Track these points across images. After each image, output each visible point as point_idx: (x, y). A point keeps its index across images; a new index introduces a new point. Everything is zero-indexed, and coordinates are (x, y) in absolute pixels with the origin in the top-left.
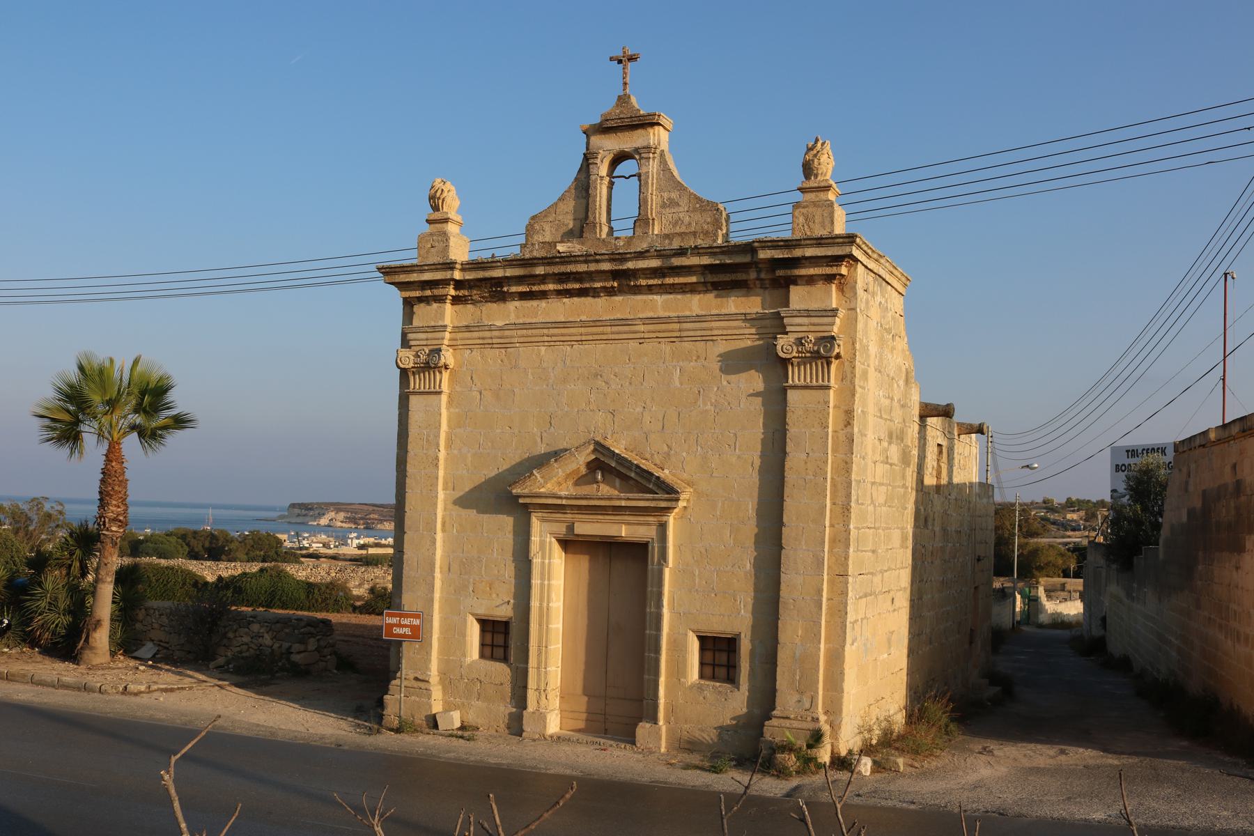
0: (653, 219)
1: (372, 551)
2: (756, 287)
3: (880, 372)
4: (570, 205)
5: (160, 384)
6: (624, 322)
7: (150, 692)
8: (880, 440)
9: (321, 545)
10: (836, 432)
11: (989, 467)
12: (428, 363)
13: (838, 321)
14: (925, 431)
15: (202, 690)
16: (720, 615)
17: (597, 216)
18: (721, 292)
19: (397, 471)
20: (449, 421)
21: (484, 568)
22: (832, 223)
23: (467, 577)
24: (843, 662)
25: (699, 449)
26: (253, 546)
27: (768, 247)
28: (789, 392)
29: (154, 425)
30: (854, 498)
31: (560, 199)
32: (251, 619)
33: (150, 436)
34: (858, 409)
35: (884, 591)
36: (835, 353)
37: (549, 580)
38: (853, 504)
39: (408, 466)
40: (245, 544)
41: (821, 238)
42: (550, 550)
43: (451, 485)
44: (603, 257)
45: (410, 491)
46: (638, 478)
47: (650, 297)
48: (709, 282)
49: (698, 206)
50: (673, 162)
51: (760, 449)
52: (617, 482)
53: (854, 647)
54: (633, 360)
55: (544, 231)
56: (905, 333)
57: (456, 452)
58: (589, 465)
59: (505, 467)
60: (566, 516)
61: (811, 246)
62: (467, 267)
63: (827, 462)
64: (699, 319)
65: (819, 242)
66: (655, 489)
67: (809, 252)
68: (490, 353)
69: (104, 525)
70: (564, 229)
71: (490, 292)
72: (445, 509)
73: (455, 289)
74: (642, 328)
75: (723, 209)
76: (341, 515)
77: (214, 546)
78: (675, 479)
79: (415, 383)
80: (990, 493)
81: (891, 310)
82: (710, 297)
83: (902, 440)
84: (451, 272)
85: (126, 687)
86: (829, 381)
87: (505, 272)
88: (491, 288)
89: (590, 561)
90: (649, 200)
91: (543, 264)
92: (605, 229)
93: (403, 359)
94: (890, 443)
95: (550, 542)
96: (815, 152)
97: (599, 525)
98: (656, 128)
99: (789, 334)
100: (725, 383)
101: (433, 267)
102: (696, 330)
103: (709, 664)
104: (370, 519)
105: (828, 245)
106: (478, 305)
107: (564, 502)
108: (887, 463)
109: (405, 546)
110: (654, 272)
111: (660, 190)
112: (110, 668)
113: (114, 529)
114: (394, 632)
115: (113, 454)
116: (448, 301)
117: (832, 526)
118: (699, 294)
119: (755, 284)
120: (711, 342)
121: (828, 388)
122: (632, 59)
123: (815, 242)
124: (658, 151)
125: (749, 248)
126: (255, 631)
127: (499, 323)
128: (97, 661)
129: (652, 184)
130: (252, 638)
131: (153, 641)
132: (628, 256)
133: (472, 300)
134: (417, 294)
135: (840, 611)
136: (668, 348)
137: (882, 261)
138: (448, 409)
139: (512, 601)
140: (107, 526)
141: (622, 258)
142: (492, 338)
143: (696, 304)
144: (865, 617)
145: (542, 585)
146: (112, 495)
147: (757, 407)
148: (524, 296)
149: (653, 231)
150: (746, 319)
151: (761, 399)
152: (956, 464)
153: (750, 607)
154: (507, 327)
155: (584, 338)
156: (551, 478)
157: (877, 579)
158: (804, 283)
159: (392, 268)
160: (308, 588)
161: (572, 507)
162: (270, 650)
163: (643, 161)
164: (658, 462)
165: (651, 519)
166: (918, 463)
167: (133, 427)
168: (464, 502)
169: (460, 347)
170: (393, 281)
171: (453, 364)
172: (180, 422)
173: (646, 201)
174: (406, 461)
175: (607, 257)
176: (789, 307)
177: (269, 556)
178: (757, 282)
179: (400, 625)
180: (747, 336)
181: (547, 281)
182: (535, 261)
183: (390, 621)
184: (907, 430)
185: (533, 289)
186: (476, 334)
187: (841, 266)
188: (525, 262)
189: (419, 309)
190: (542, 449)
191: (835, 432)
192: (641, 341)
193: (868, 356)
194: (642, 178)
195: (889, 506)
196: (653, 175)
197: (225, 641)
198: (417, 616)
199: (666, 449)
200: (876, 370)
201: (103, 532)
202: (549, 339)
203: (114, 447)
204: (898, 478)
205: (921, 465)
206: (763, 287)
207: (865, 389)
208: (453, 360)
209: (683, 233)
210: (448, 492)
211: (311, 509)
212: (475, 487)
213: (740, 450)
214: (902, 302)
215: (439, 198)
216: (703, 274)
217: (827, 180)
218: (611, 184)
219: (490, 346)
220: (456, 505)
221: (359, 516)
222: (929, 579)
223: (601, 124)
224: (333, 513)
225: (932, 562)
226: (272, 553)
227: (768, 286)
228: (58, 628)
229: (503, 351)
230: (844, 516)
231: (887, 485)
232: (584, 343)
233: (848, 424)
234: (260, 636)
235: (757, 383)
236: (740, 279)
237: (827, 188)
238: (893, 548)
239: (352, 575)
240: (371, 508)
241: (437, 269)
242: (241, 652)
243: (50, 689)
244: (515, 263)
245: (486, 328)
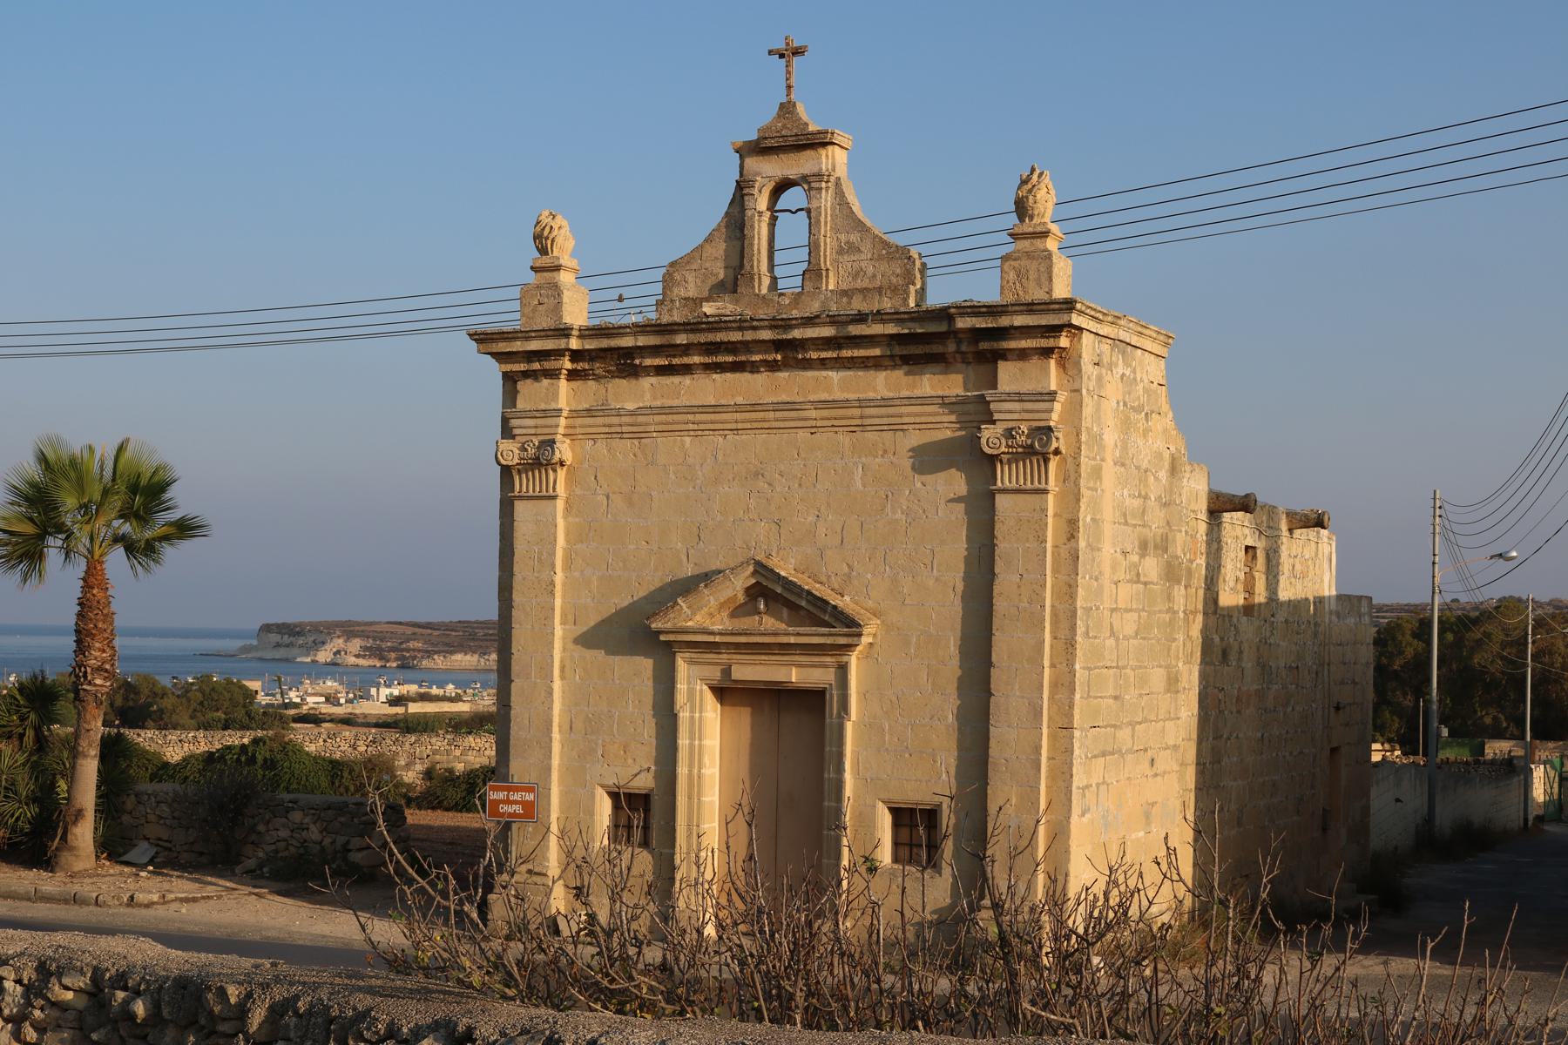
0: (827, 270)
1: (414, 708)
3: (1123, 465)
4: (719, 248)
5: (156, 479)
6: (790, 406)
7: (165, 903)
8: (1124, 553)
9: (323, 699)
10: (1057, 547)
11: (1437, 558)
12: (538, 458)
13: (1057, 406)
14: (1219, 530)
15: (234, 899)
16: (916, 781)
17: (755, 264)
18: (912, 368)
20: (567, 534)
21: (615, 726)
22: (1050, 280)
23: (594, 737)
24: (1069, 837)
25: (887, 568)
26: (201, 703)
27: (967, 313)
28: (998, 497)
29: (148, 534)
30: (1080, 630)
31: (706, 240)
32: (290, 805)
33: (142, 551)
34: (1086, 517)
35: (1136, 748)
36: (1052, 448)
37: (700, 739)
38: (1079, 638)
39: (514, 593)
40: (189, 700)
41: (1033, 304)
42: (701, 700)
43: (571, 617)
44: (762, 323)
45: (518, 626)
47: (824, 373)
49: (884, 252)
50: (853, 191)
51: (963, 569)
52: (785, 612)
53: (1084, 820)
54: (803, 455)
55: (686, 282)
56: (1168, 406)
57: (577, 574)
58: (748, 590)
59: (642, 594)
60: (721, 656)
61: (1021, 312)
62: (588, 333)
63: (1045, 585)
64: (885, 402)
65: (1031, 308)
66: (831, 621)
67: (1019, 321)
68: (616, 443)
69: (85, 676)
70: (712, 281)
71: (618, 365)
72: (564, 650)
73: (572, 361)
74: (813, 414)
75: (916, 256)
76: (356, 645)
77: (131, 703)
78: (857, 608)
79: (521, 484)
81: (1142, 381)
82: (898, 375)
83: (1166, 550)
84: (565, 340)
85: (132, 897)
86: (1046, 483)
87: (636, 340)
88: (619, 360)
89: (752, 714)
90: (822, 244)
91: (686, 331)
92: (766, 281)
93: (504, 454)
94: (1143, 556)
95: (701, 691)
96: (1030, 186)
97: (762, 666)
98: (830, 148)
99: (998, 423)
100: (919, 485)
101: (542, 334)
102: (882, 417)
103: (905, 844)
104: (408, 650)
106: (603, 381)
107: (718, 639)
108: (1138, 582)
109: (513, 699)
110: (828, 343)
111: (836, 230)
112: (98, 875)
113: (98, 682)
115: (92, 579)
116: (562, 376)
117: (1053, 666)
118: (886, 370)
119: (954, 358)
120: (901, 433)
121: (1045, 492)
122: (798, 52)
123: (1025, 308)
124: (832, 179)
125: (944, 314)
126: (297, 821)
127: (630, 406)
128: (79, 866)
129: (826, 223)
130: (292, 831)
131: (148, 839)
132: (794, 322)
133: (594, 374)
134: (522, 367)
135: (1063, 774)
136: (847, 440)
137: (1122, 322)
138: (565, 518)
139: (653, 768)
140: (89, 678)
141: (787, 325)
142: (621, 425)
143: (883, 383)
144: (1103, 783)
145: (691, 746)
146: (94, 635)
147: (959, 516)
148: (661, 371)
149: (827, 285)
150: (944, 404)
151: (963, 505)
152: (1286, 571)
153: (953, 771)
154: (639, 412)
155: (740, 426)
156: (700, 609)
157: (1124, 734)
158: (1015, 357)
159: (487, 334)
160: (333, 768)
161: (728, 645)
162: (318, 847)
163: (813, 193)
164: (836, 586)
165: (828, 659)
166: (1206, 577)
167: (118, 539)
168: (587, 640)
169: (580, 437)
170: (490, 350)
171: (570, 459)
172: (185, 529)
173: (817, 246)
174: (512, 588)
175: (766, 323)
176: (996, 389)
177: (234, 721)
178: (957, 355)
179: (508, 802)
180: (946, 425)
181: (691, 352)
182: (676, 328)
184: (1175, 536)
185: (674, 363)
186: (600, 421)
187: (1059, 337)
188: (662, 328)
189: (525, 387)
190: (689, 570)
191: (1055, 547)
193: (1102, 448)
194: (813, 214)
196: (826, 210)
197: (254, 837)
198: (530, 790)
199: (846, 569)
200: (1115, 464)
201: (85, 687)
202: (695, 427)
203: (95, 568)
204: (1159, 600)
205: (1212, 579)
206: (965, 362)
207: (1097, 491)
208: (571, 454)
209: (865, 289)
210: (567, 627)
211: (299, 634)
212: (603, 621)
213: (938, 571)
214: (1163, 367)
215: (547, 238)
216: (889, 345)
217: (1044, 224)
218: (773, 219)
219: (620, 436)
220: (577, 644)
221: (389, 644)
222: (1235, 735)
223: (757, 142)
224: (341, 641)
225: (1239, 712)
226: (240, 714)
227: (971, 360)
228: (20, 823)
229: (636, 442)
231: (1138, 611)
232: (740, 432)
233: (1072, 536)
234: (303, 828)
235: (960, 486)
237: (1045, 234)
238: (1152, 693)
239: (394, 748)
240: (409, 630)
241: (547, 337)
242: (277, 852)
243: (25, 903)
244: (648, 329)
245: (614, 412)
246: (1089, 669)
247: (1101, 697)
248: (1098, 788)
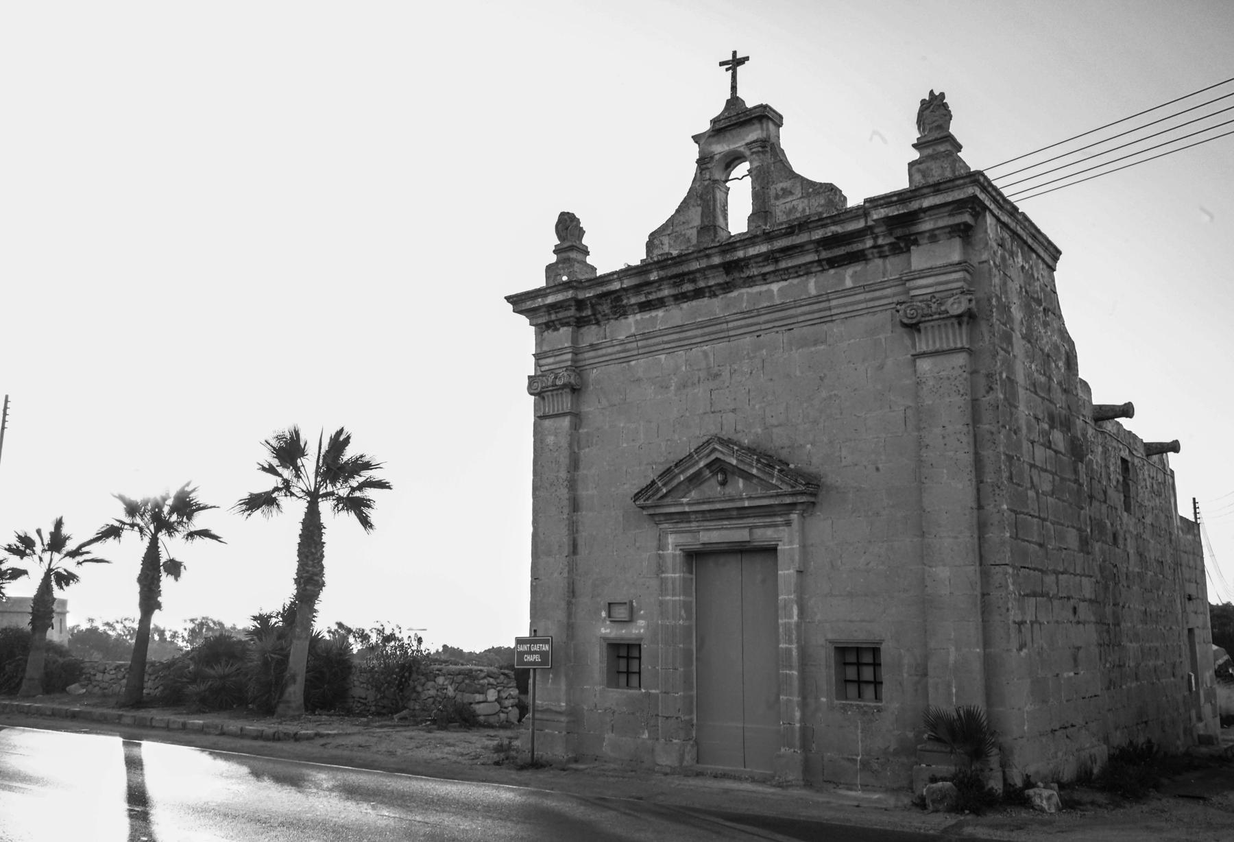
2: (874, 257)
41: (939, 184)
46: (760, 475)
48: (824, 260)
49: (811, 190)
53: (1022, 653)
66: (779, 483)
80: (1196, 532)
98: (764, 121)
101: (555, 289)
105: (947, 190)
108: (1050, 448)
110: (770, 257)
130: (438, 690)
157: (1050, 579)
179: (530, 653)
192: (758, 333)
195: (1058, 499)
207: (1009, 354)
225: (1128, 587)
227: (887, 253)
234: (444, 688)
236: (855, 250)
246: (1016, 513)
247: (1027, 541)
248: (1032, 625)
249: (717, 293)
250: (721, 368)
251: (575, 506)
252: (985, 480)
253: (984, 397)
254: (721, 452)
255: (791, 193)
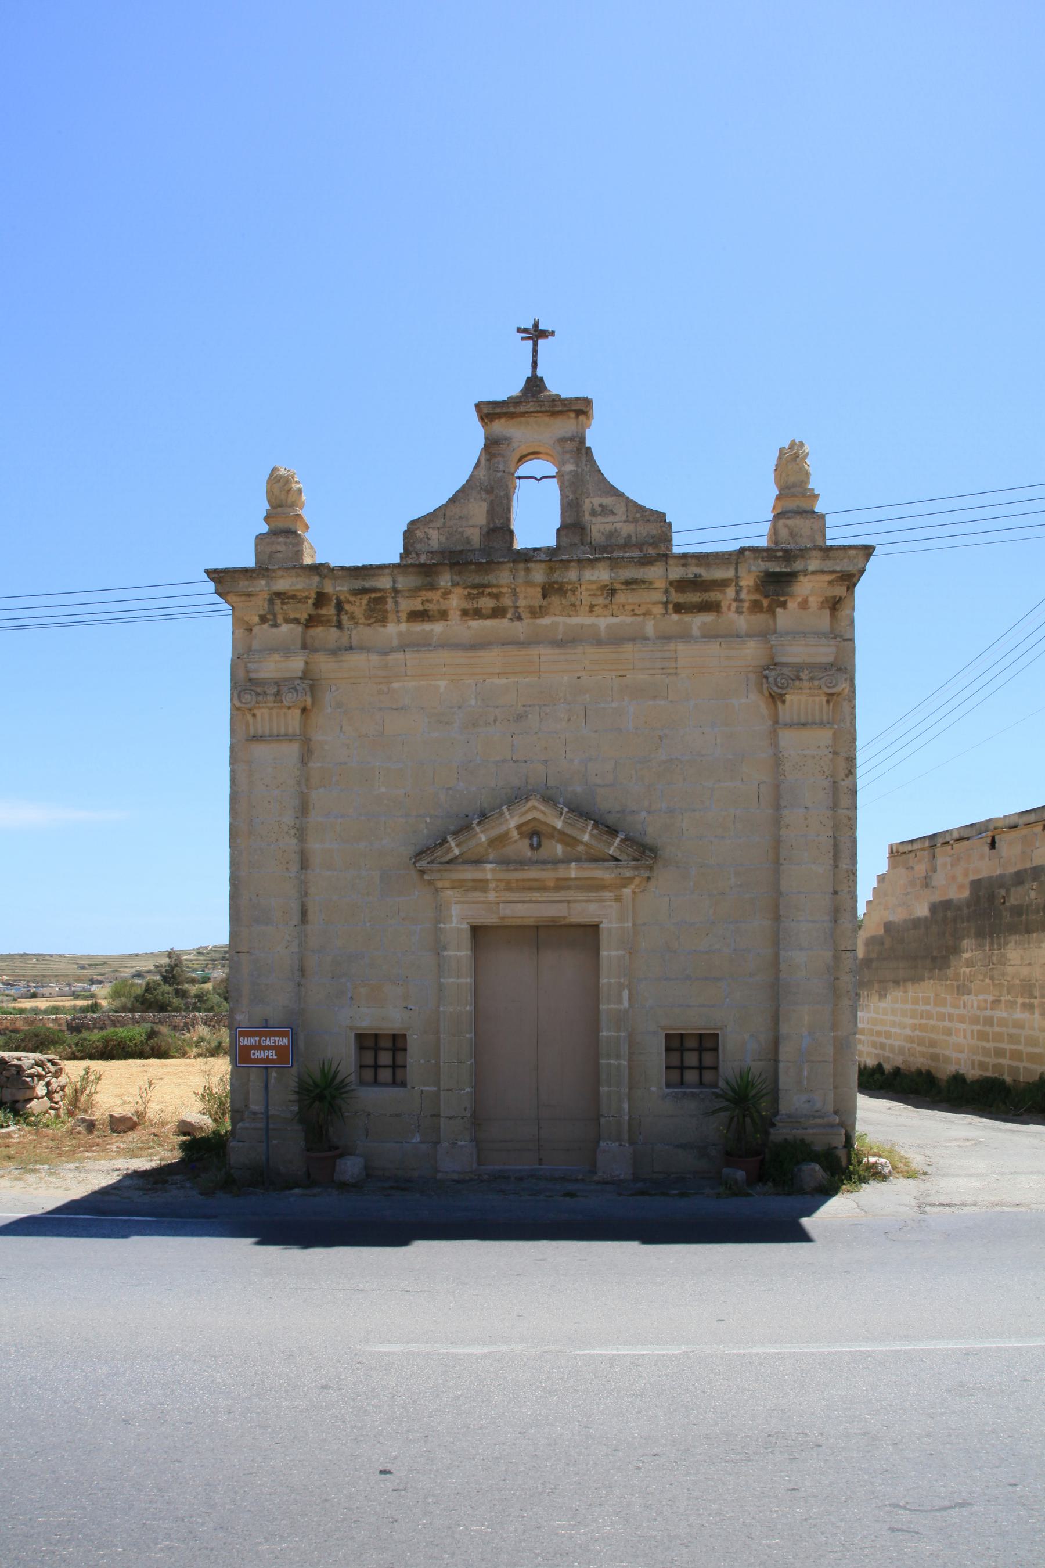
19: (230, 847)
49: (638, 515)
114: (253, 1057)
179: (260, 1047)
183: (246, 1043)
230: (849, 880)
249: (523, 616)
250: (528, 709)
251: (304, 863)
252: (840, 866)
253: (843, 780)
254: (542, 812)
255: (612, 513)
